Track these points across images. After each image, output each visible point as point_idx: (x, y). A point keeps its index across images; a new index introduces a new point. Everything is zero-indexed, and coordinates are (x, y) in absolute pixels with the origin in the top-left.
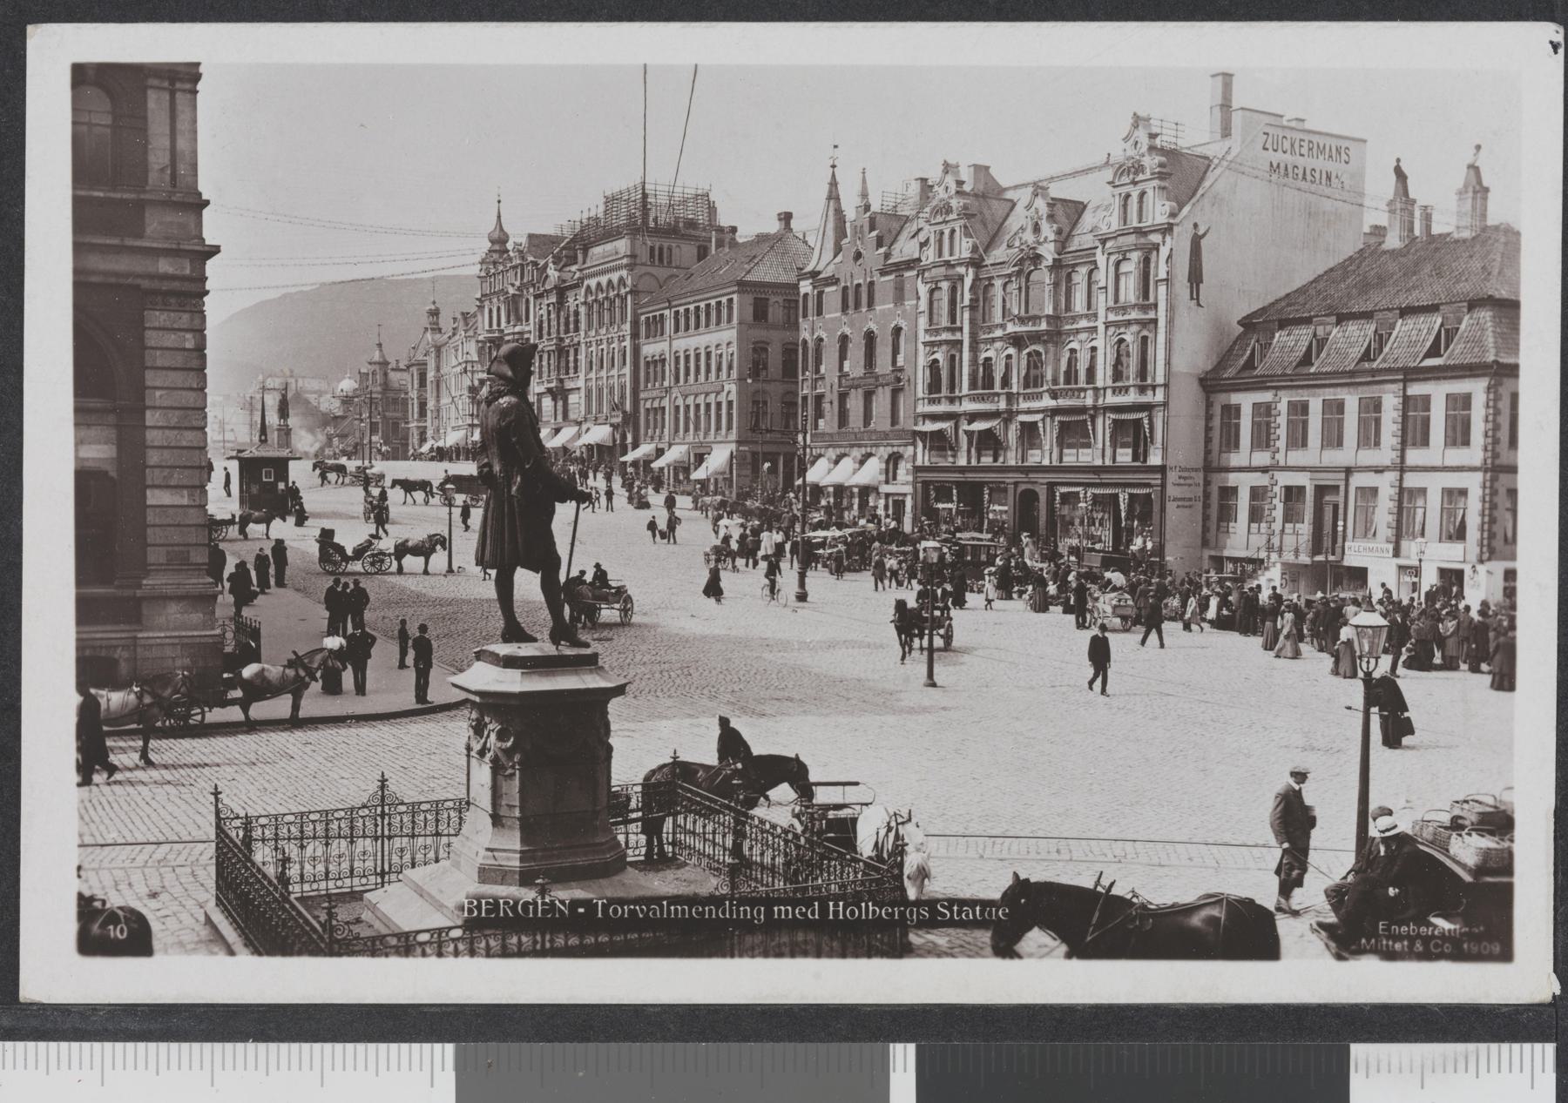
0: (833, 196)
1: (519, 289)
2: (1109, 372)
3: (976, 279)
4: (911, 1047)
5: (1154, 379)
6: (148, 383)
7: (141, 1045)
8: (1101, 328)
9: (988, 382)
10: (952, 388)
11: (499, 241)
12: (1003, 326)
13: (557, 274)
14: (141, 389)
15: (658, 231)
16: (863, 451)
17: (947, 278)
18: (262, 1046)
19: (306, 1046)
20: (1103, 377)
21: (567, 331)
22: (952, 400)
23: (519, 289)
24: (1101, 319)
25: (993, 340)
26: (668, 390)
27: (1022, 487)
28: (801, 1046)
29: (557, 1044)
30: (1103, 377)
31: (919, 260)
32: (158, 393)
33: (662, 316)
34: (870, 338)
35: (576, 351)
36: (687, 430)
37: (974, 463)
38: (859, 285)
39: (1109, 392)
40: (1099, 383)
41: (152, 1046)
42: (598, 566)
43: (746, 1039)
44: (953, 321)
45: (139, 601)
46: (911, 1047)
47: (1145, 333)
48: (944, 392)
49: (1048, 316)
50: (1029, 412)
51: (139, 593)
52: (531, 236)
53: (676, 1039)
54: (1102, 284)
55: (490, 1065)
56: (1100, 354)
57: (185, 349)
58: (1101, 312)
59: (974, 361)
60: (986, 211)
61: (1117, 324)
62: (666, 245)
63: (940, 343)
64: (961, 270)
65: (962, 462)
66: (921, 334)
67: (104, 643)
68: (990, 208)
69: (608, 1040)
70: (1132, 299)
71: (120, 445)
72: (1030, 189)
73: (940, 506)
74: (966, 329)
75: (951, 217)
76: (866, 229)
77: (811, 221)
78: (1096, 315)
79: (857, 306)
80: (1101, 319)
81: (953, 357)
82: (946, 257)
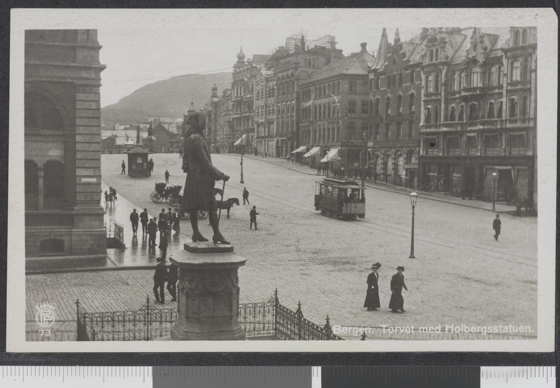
0: (384, 35)
1: (249, 79)
2: (508, 112)
4: (320, 368)
6: (77, 124)
7: (37, 367)
8: (505, 93)
9: (452, 118)
11: (241, 57)
12: (460, 93)
14: (74, 126)
15: (310, 52)
16: (396, 149)
18: (82, 367)
19: (98, 367)
20: (505, 114)
22: (436, 126)
23: (249, 79)
24: (505, 88)
25: (455, 99)
26: (312, 123)
28: (279, 367)
29: (190, 367)
30: (505, 114)
31: (422, 63)
32: (81, 128)
33: (309, 89)
36: (319, 140)
37: (446, 155)
38: (395, 75)
39: (508, 122)
40: (504, 118)
41: (41, 367)
42: (111, 188)
43: (259, 365)
45: (74, 215)
46: (320, 368)
47: (525, 94)
48: (433, 122)
49: (480, 88)
50: (471, 131)
51: (73, 213)
52: (254, 56)
53: (233, 365)
54: (505, 72)
55: (165, 374)
56: (504, 104)
57: (92, 109)
58: (505, 85)
59: (446, 109)
60: (453, 41)
61: (512, 91)
62: (308, 58)
63: (431, 100)
64: (441, 67)
66: (423, 96)
67: (59, 233)
68: (454, 39)
69: (209, 365)
70: (519, 79)
71: (66, 150)
72: (473, 30)
73: (431, 174)
74: (443, 94)
75: (437, 43)
77: (373, 48)
80: (505, 88)
82: (434, 61)
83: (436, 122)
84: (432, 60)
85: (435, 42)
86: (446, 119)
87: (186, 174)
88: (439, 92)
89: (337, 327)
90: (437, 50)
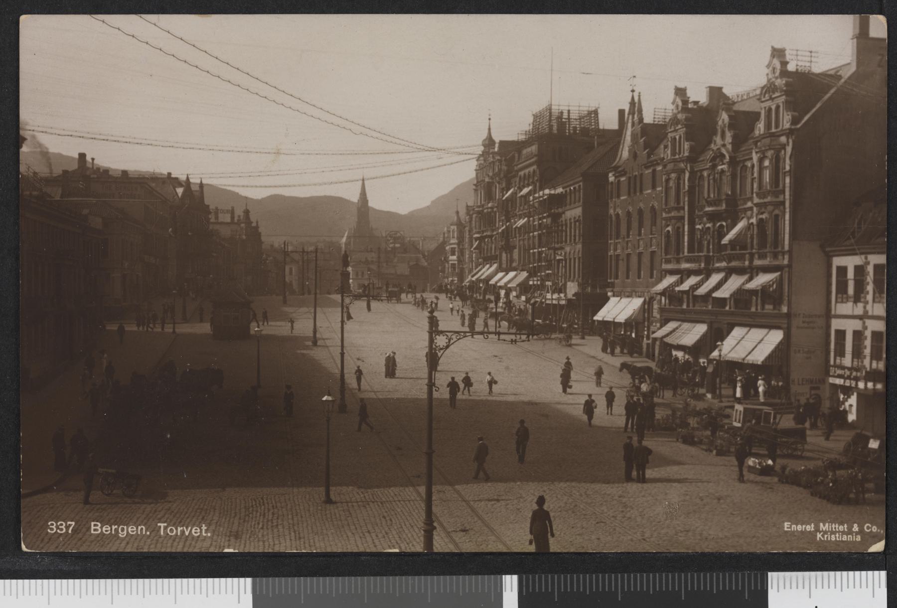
1: (492, 178)
3: (692, 173)
5: (783, 247)
34: (640, 212)
37: (691, 308)
47: (777, 212)
76: (639, 135)
79: (635, 192)
82: (773, 130)
83: (776, 247)
85: (774, 93)
86: (691, 249)
88: (682, 204)
89: (95, 525)
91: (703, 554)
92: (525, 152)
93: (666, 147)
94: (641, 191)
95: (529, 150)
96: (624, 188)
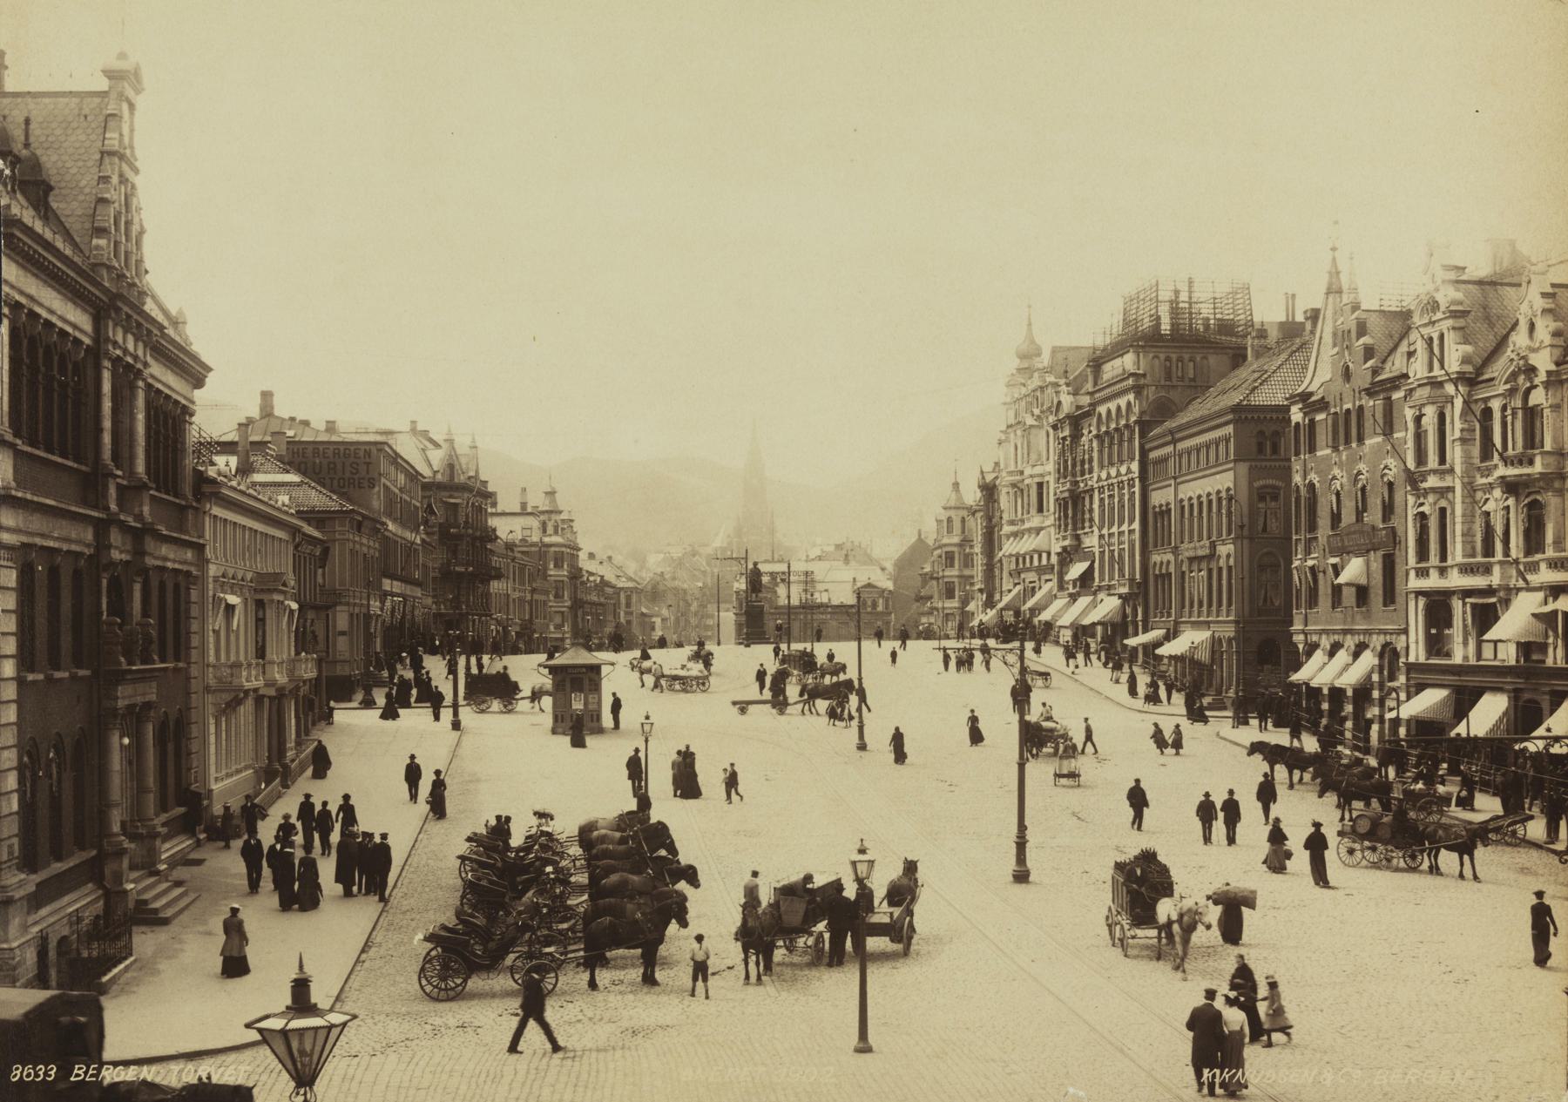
10: (1443, 558)
13: (1070, 398)
16: (1357, 639)
17: (1431, 401)
21: (1083, 474)
27: (1527, 696)
31: (1406, 376)
35: (1091, 497)
38: (1348, 411)
44: (1442, 460)
47: (1443, 503)
59: (1469, 518)
65: (1457, 659)
75: (1439, 315)
76: (1354, 334)
78: (1451, 471)
79: (1347, 442)
81: (1443, 511)
84: (1431, 369)
87: (1191, 1034)
90: (1442, 337)
91: (696, 775)
92: (1107, 367)
93: (1410, 354)
94: (1361, 440)
95: (1117, 362)
96: (1322, 436)
